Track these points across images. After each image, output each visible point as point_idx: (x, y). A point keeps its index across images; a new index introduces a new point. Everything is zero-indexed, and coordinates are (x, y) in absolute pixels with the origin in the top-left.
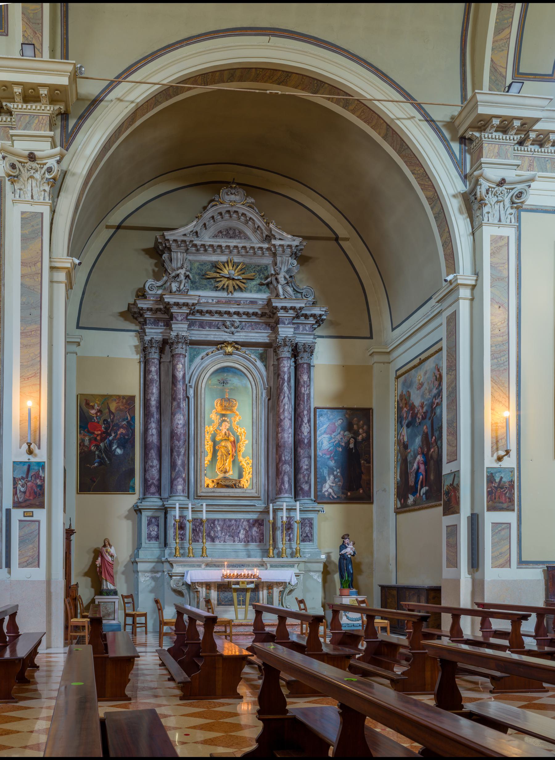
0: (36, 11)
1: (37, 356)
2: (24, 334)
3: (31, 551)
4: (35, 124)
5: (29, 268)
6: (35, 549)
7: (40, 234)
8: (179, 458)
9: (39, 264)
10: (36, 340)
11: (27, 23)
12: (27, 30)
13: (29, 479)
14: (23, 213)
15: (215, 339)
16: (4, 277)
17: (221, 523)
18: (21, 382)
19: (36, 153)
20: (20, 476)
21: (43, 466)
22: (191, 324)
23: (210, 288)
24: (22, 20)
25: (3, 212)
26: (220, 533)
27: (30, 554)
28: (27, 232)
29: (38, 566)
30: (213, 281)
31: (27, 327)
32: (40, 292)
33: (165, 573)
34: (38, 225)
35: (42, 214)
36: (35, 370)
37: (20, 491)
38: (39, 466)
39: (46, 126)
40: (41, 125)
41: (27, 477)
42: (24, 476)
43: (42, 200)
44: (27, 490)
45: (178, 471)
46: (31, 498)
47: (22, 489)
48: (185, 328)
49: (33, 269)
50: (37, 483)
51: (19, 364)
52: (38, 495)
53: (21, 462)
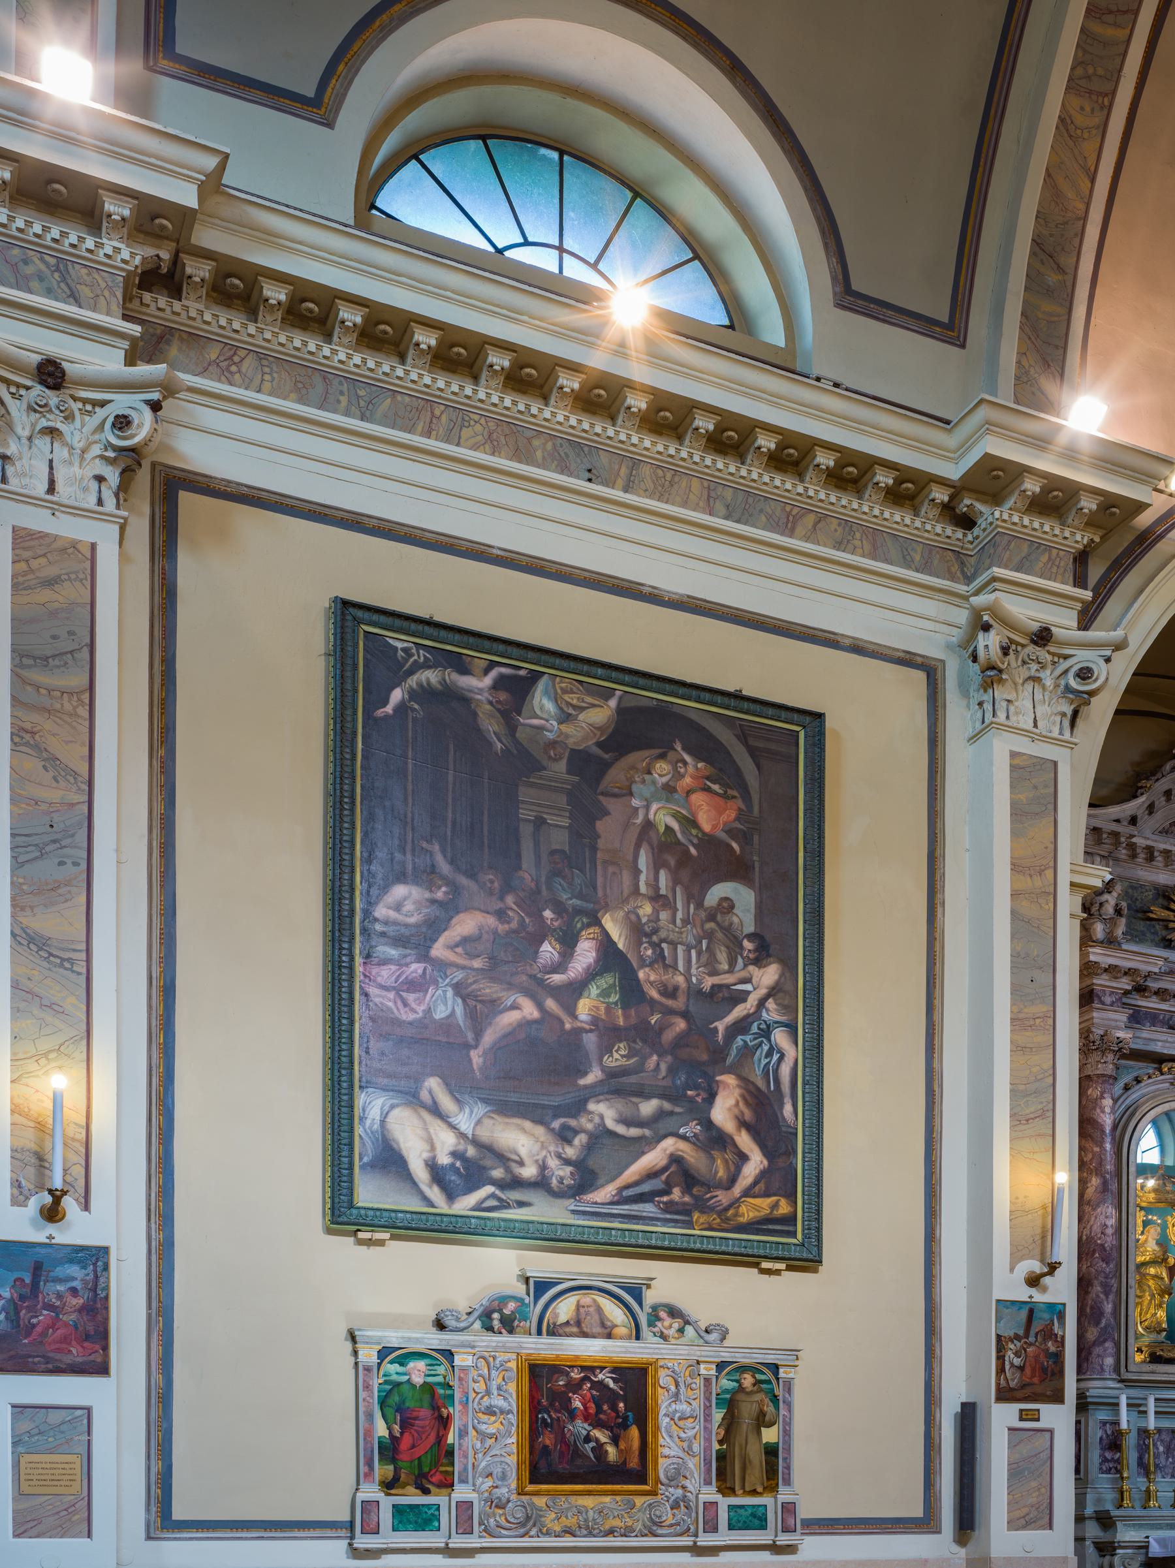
0: (1056, 319)
1: (1046, 1074)
2: (1017, 1022)
3: (1034, 1495)
4: (1041, 565)
5: (1029, 879)
6: (1043, 1490)
7: (1051, 807)
8: (1107, 1298)
9: (1049, 873)
10: (1045, 1039)
11: (1030, 338)
12: (1028, 354)
13: (1032, 1339)
14: (1014, 755)
15: (1165, 1052)
16: (944, 887)
17: (1164, 1436)
18: (1012, 1127)
19: (1053, 628)
20: (1011, 1334)
21: (1060, 1312)
22: (1137, 1018)
23: (1152, 941)
24: (1020, 328)
25: (939, 739)
26: (1162, 1459)
27: (1032, 1500)
28: (1023, 797)
29: (1050, 1526)
30: (1157, 927)
31: (1025, 1006)
32: (1052, 934)
33: (1087, 1543)
34: (1046, 786)
35: (1055, 764)
36: (1042, 1103)
37: (1012, 1365)
38: (1052, 1313)
39: (1067, 575)
40: (1054, 570)
41: (1027, 1335)
42: (1021, 1332)
43: (1055, 734)
44: (1028, 1364)
45: (1106, 1327)
46: (1036, 1380)
47: (1017, 1361)
48: (1120, 1021)
49: (1038, 882)
50: (1048, 1349)
51: (1008, 1087)
52: (1049, 1374)
53: (1013, 1302)
